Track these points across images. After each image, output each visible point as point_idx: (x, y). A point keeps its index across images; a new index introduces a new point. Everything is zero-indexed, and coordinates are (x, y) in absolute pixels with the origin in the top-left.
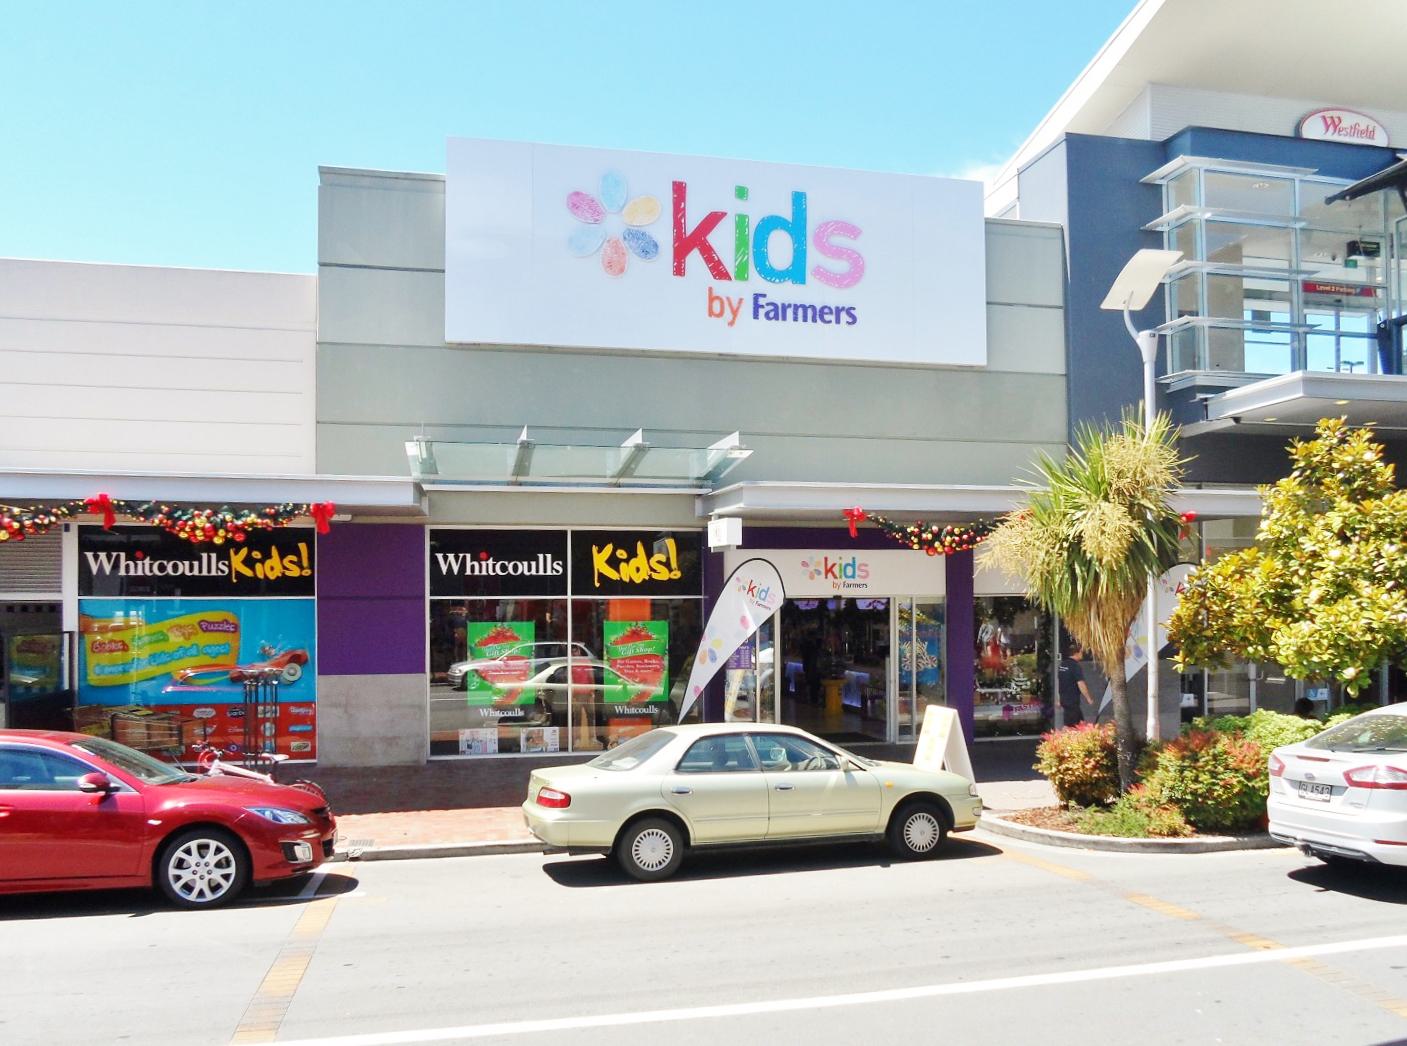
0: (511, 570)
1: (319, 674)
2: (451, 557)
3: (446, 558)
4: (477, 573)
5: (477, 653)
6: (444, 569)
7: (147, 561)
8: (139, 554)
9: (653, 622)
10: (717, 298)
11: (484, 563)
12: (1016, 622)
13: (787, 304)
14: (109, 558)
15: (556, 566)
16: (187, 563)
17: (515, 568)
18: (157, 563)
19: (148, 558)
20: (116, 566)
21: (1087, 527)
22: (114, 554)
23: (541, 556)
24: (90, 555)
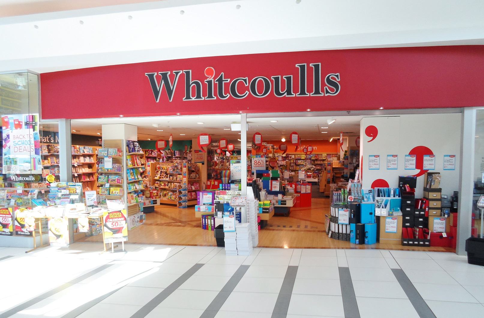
7: (21, 177)
23: (30, 176)
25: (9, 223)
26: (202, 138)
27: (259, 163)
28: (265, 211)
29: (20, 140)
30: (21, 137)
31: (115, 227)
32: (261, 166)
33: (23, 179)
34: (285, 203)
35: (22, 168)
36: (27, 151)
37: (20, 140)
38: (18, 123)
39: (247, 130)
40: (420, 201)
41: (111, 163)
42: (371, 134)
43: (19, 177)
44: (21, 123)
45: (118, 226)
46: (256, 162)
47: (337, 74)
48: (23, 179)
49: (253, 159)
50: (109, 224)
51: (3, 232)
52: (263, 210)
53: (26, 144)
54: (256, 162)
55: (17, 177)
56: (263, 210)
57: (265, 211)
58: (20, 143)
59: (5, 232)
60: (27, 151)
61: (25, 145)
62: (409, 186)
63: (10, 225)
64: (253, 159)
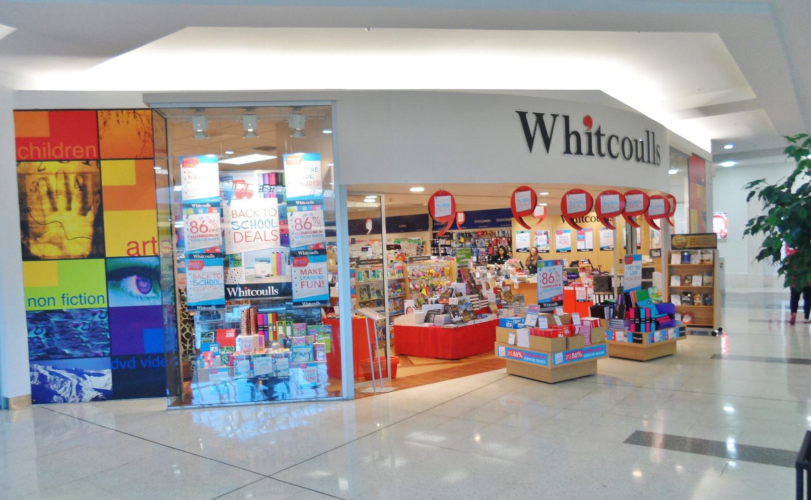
0: (257, 294)
1: (383, 378)
2: (233, 289)
3: (231, 290)
4: (243, 295)
5: (717, 353)
6: (230, 294)
7: (249, 290)
8: (246, 288)
9: (353, 390)
10: (553, 277)
11: (246, 291)
12: (641, 283)
13: (146, 241)
14: (235, 290)
15: (275, 291)
16: (263, 291)
17: (259, 293)
18: (253, 291)
19: (249, 290)
20: (238, 292)
21: (527, 235)
22: (237, 288)
23: (269, 287)
24: (228, 289)
26: (673, 284)
27: (551, 279)
29: (247, 219)
32: (556, 285)
33: (254, 293)
34: (640, 339)
35: (251, 272)
36: (263, 239)
37: (247, 219)
42: (199, 131)
43: (244, 290)
46: (545, 276)
48: (254, 293)
49: (291, 215)
53: (268, 226)
54: (545, 276)
55: (242, 290)
60: (263, 239)
61: (258, 229)
64: (291, 215)
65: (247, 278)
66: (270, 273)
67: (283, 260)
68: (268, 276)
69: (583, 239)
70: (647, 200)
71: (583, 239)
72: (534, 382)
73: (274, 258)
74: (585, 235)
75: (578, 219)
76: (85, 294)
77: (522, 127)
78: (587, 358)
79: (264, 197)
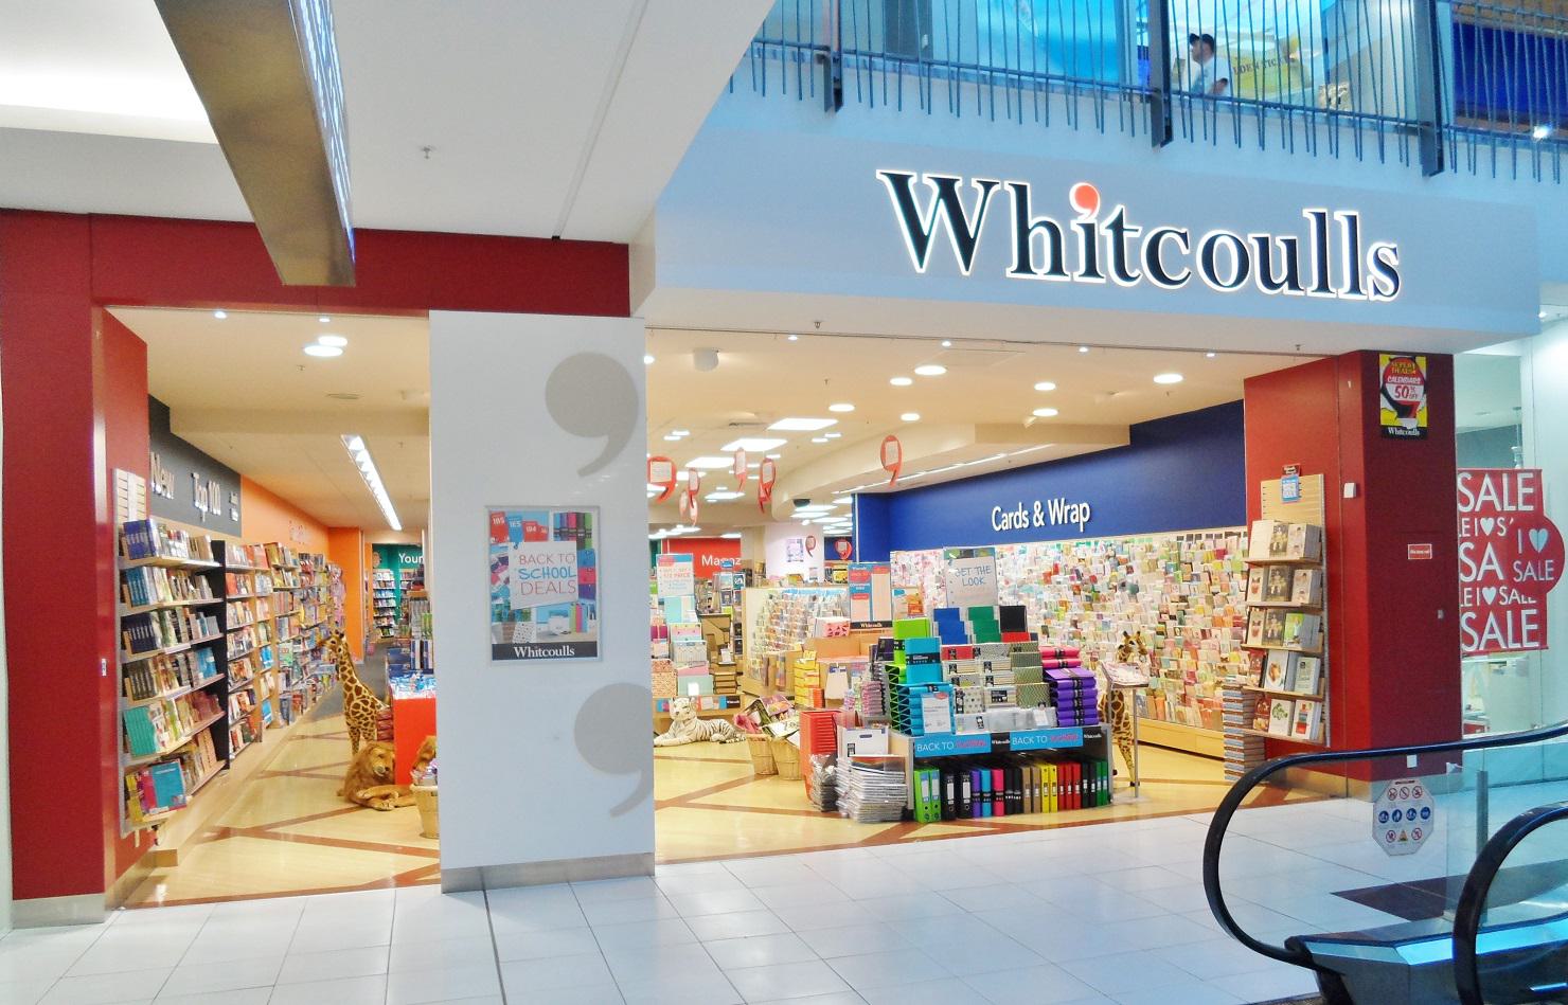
2: (521, 648)
25: (1417, 400)
28: (1091, 737)
29: (540, 567)
30: (545, 559)
31: (1401, 399)
36: (558, 590)
38: (535, 529)
39: (725, 488)
40: (1520, 551)
41: (692, 583)
44: (544, 531)
45: (1408, 399)
47: (1183, 231)
50: (1391, 389)
51: (1399, 428)
52: (993, 742)
56: (993, 742)
57: (1091, 737)
58: (536, 574)
59: (1405, 429)
60: (558, 590)
62: (646, 453)
63: (1420, 407)
65: (539, 635)
66: (568, 629)
67: (584, 613)
68: (565, 633)
69: (865, 594)
70: (524, 524)
71: (865, 594)
72: (797, 83)
73: (572, 611)
74: (870, 582)
75: (1056, 501)
76: (661, 603)
77: (61, 130)
78: (845, 495)
79: (811, 569)
